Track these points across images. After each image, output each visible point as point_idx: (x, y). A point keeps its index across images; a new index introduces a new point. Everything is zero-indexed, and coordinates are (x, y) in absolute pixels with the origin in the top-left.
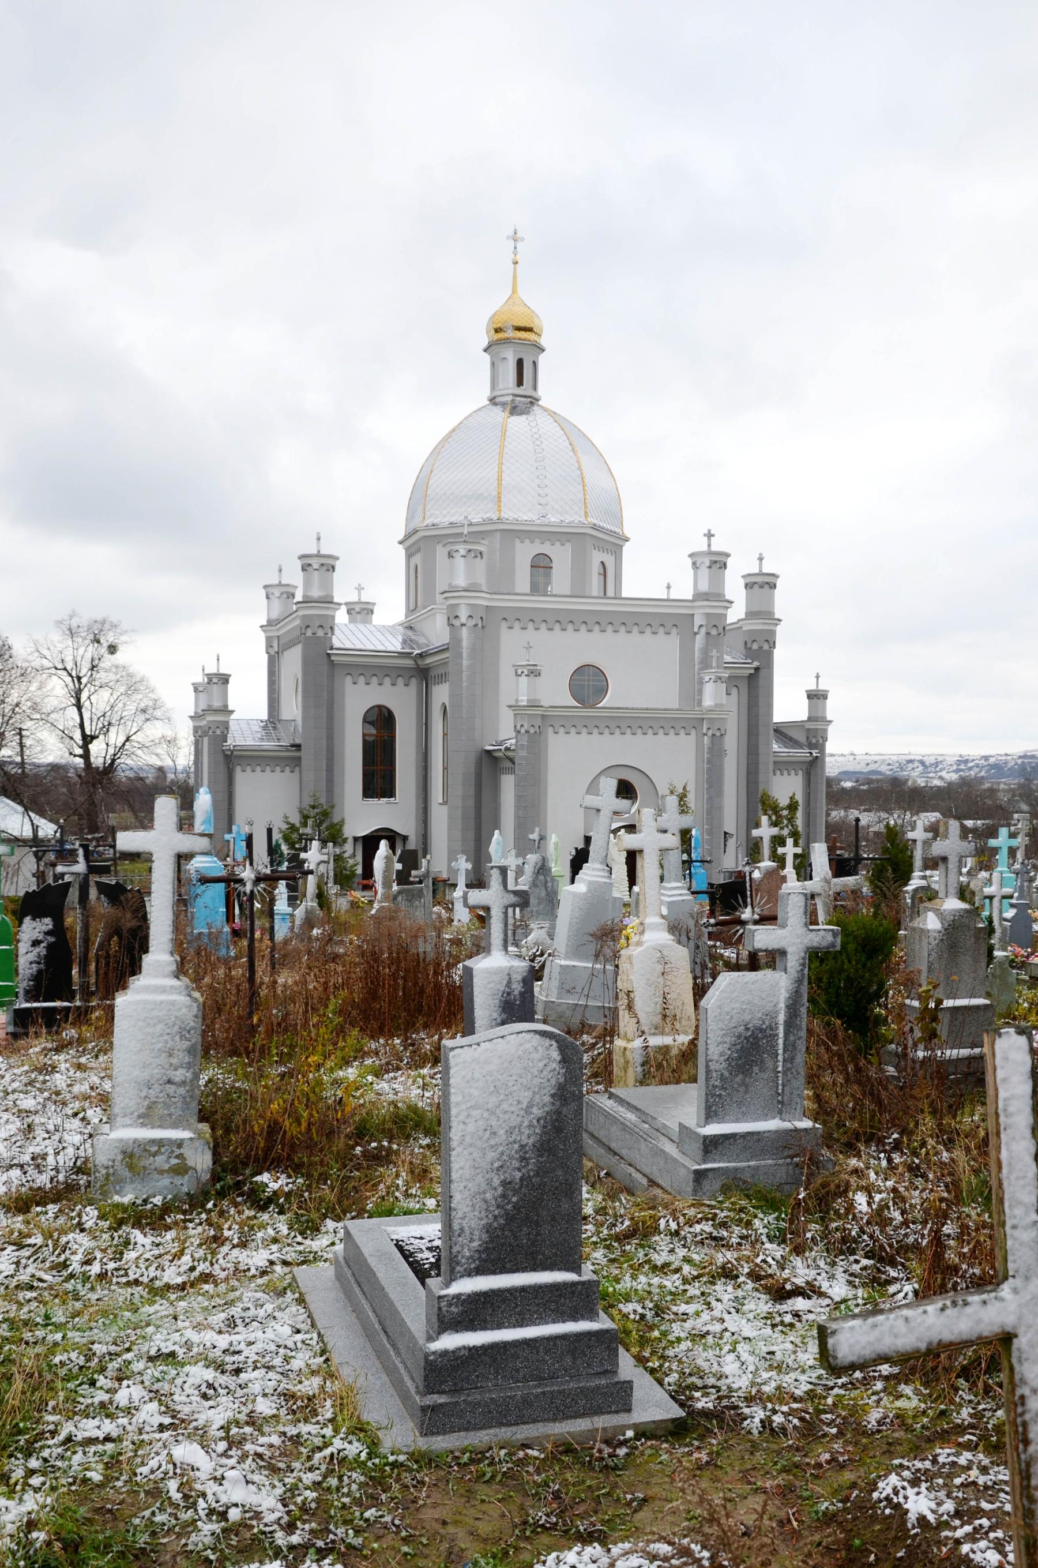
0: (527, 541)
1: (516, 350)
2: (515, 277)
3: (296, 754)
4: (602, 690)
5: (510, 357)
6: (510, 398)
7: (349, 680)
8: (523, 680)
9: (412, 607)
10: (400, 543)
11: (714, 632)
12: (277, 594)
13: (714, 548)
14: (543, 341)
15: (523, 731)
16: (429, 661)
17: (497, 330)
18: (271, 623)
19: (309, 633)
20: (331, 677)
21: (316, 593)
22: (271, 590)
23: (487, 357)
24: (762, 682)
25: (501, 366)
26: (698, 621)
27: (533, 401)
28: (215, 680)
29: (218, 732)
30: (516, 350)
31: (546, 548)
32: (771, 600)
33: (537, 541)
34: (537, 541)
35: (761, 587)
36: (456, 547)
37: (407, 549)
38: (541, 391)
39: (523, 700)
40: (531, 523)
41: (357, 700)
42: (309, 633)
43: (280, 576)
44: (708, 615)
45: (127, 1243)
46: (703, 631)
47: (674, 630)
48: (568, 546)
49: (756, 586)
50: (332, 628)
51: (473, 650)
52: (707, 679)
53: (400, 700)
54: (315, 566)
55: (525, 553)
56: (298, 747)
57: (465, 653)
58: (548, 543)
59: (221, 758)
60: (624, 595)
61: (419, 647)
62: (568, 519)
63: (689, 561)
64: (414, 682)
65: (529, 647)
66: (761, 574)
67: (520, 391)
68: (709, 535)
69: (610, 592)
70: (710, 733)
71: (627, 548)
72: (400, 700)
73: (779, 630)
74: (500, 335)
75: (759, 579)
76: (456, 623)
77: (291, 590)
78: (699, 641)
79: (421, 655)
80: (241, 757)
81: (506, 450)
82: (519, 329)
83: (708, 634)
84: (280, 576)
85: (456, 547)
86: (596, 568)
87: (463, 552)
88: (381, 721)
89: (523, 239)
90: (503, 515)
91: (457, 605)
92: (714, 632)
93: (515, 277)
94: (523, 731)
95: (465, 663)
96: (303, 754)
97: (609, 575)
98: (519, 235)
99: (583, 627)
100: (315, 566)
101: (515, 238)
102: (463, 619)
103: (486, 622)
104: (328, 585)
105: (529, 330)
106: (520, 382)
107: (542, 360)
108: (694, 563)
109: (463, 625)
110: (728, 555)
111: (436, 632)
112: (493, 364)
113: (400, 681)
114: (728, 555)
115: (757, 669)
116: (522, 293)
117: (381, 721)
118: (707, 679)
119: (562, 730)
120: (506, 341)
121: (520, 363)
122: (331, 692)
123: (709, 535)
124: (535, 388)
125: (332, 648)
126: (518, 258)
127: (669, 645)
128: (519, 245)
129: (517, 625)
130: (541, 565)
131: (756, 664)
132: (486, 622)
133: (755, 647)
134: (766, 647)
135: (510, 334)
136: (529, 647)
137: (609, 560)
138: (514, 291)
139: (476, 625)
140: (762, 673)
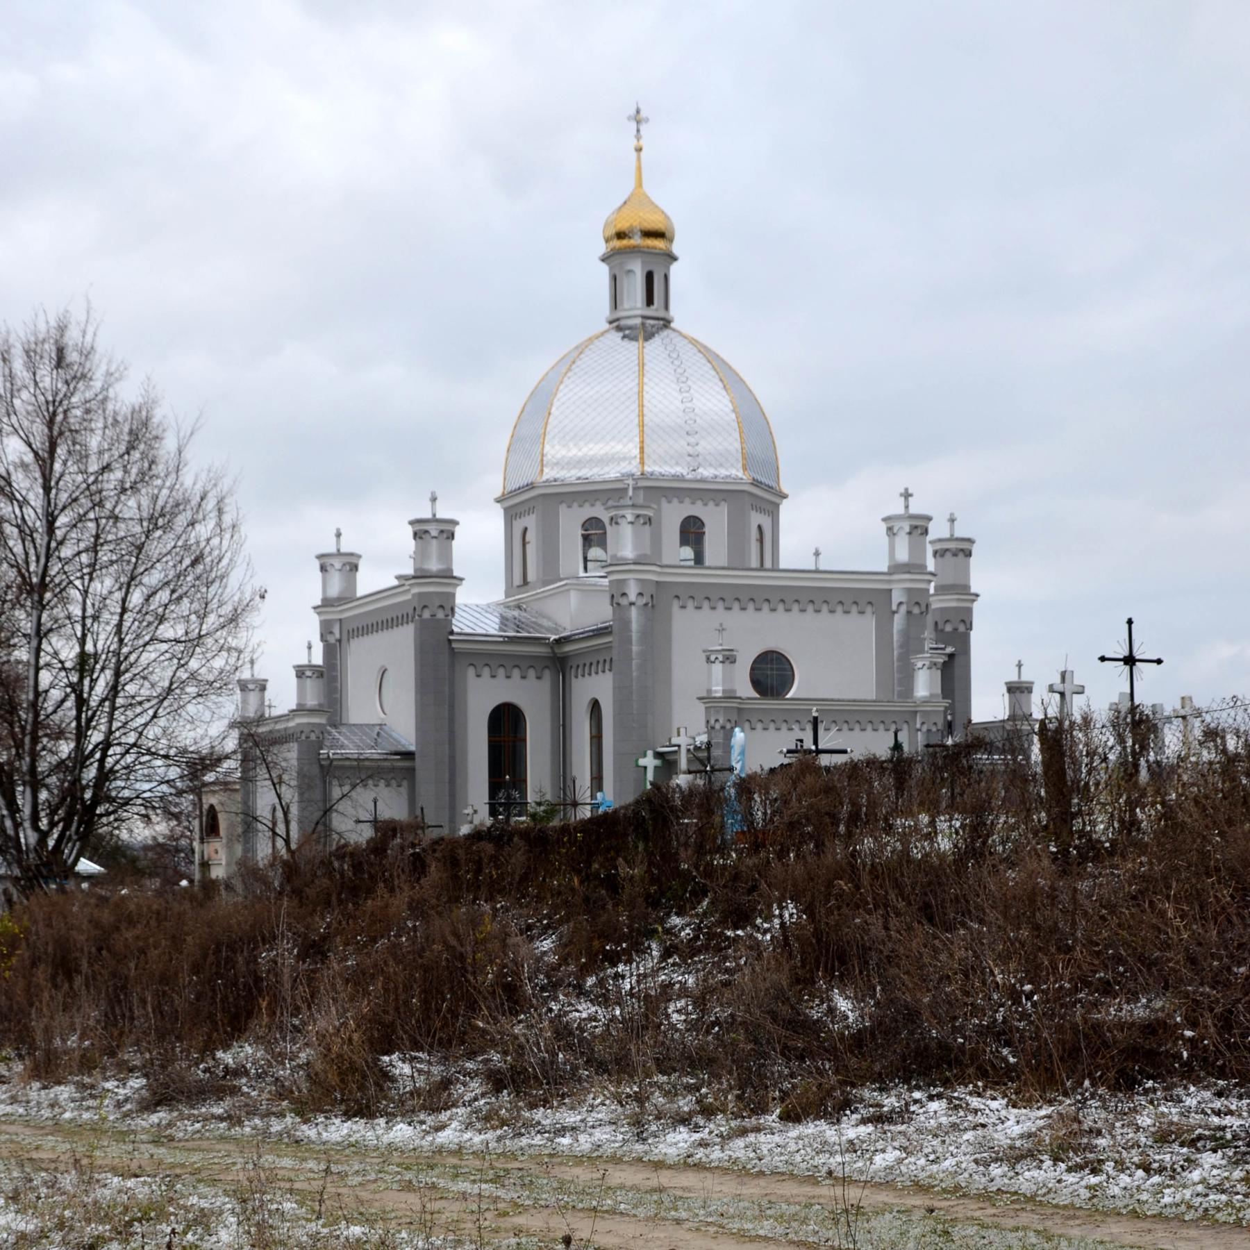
0: (675, 501)
1: (641, 255)
2: (639, 169)
3: (406, 764)
4: (786, 679)
5: (638, 269)
6: (638, 321)
7: (471, 672)
8: (718, 668)
9: (518, 580)
10: (498, 501)
11: (916, 610)
12: (338, 565)
13: (913, 511)
14: (676, 249)
15: (718, 726)
16: (568, 648)
17: (620, 235)
18: (327, 603)
19: (426, 614)
20: (452, 666)
21: (434, 566)
22: (325, 560)
23: (604, 269)
24: (958, 671)
25: (624, 282)
26: (897, 597)
27: (666, 323)
28: (308, 673)
29: (313, 737)
30: (641, 255)
31: (697, 510)
32: (966, 571)
33: (687, 500)
34: (687, 500)
35: (955, 555)
36: (621, 512)
37: (506, 510)
38: (675, 311)
39: (718, 690)
40: (680, 478)
41: (482, 696)
42: (426, 614)
43: (338, 542)
44: (909, 591)
45: (1014, 898)
46: (903, 609)
47: (869, 609)
48: (724, 508)
49: (948, 555)
50: (453, 610)
51: (646, 635)
52: (920, 664)
53: (534, 697)
54: (434, 533)
55: (673, 515)
56: (408, 755)
57: (635, 637)
58: (699, 503)
59: (315, 770)
60: (782, 565)
61: (555, 631)
62: (723, 472)
63: (884, 526)
64: (547, 674)
65: (721, 630)
66: (952, 539)
67: (650, 312)
68: (907, 495)
69: (768, 564)
70: (925, 728)
71: (785, 509)
72: (534, 697)
73: (977, 607)
74: (625, 242)
75: (952, 545)
76: (624, 602)
77: (353, 560)
78: (898, 621)
79: (558, 642)
80: (342, 767)
81: (646, 388)
82: (648, 234)
83: (909, 612)
84: (338, 542)
85: (621, 512)
86: (754, 534)
87: (630, 518)
88: (506, 723)
89: (647, 120)
90: (647, 469)
91: (624, 580)
92: (916, 610)
93: (639, 169)
94: (718, 726)
95: (635, 649)
96: (418, 762)
97: (767, 539)
98: (643, 114)
99: (766, 607)
100: (434, 533)
101: (638, 118)
102: (632, 597)
103: (659, 599)
104: (446, 555)
105: (659, 235)
106: (650, 301)
107: (675, 270)
108: (890, 529)
109: (632, 604)
110: (929, 519)
111: (571, 611)
112: (614, 279)
113: (532, 673)
114: (929, 519)
115: (951, 656)
116: (648, 188)
117: (506, 723)
118: (920, 664)
119: (759, 726)
120: (634, 250)
121: (649, 277)
122: (452, 684)
123: (907, 495)
124: (667, 307)
125: (452, 633)
126: (642, 142)
127: (864, 626)
128: (642, 128)
129: (690, 604)
130: (692, 532)
131: (950, 650)
132: (659, 599)
133: (948, 628)
134: (962, 628)
135: (637, 241)
136: (721, 630)
137: (766, 522)
138: (639, 183)
139: (646, 605)
140: (958, 661)
